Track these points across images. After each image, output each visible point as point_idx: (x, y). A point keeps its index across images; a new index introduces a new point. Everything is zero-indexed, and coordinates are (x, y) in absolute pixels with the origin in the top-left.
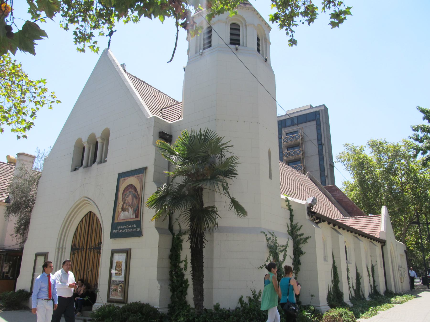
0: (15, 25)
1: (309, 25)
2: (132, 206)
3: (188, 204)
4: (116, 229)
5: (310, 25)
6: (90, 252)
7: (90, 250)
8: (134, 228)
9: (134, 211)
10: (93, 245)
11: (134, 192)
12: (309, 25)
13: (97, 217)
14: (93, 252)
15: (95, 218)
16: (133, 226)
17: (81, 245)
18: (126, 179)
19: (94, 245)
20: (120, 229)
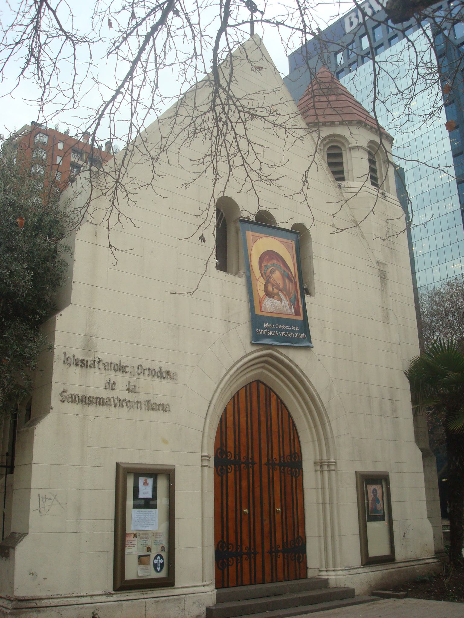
0: (19, 10)
1: (112, 28)
2: (285, 293)
3: (451, 350)
4: (261, 327)
5: (113, 26)
6: (271, 472)
7: (270, 466)
8: (294, 331)
9: (291, 301)
10: (276, 456)
11: (283, 268)
12: (112, 28)
13: (278, 397)
14: (278, 471)
15: (274, 399)
16: (294, 328)
17: (243, 454)
18: (261, 237)
19: (280, 457)
20: (269, 329)
